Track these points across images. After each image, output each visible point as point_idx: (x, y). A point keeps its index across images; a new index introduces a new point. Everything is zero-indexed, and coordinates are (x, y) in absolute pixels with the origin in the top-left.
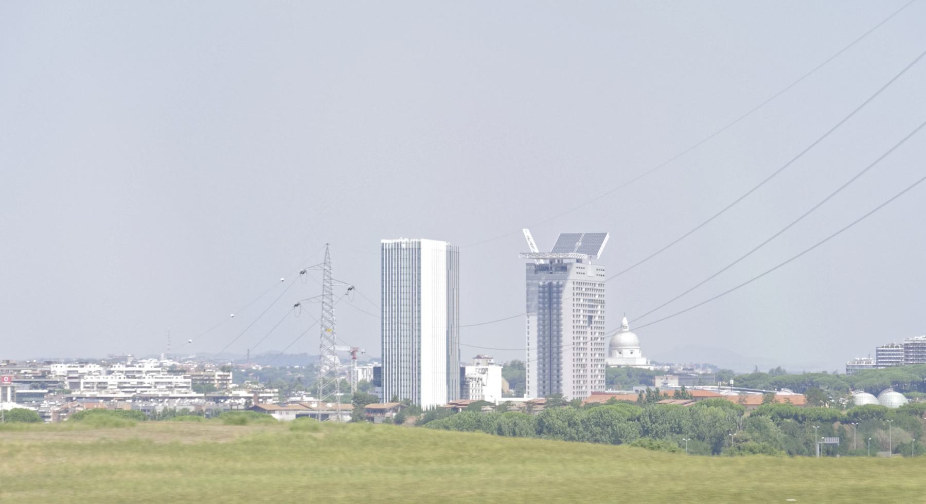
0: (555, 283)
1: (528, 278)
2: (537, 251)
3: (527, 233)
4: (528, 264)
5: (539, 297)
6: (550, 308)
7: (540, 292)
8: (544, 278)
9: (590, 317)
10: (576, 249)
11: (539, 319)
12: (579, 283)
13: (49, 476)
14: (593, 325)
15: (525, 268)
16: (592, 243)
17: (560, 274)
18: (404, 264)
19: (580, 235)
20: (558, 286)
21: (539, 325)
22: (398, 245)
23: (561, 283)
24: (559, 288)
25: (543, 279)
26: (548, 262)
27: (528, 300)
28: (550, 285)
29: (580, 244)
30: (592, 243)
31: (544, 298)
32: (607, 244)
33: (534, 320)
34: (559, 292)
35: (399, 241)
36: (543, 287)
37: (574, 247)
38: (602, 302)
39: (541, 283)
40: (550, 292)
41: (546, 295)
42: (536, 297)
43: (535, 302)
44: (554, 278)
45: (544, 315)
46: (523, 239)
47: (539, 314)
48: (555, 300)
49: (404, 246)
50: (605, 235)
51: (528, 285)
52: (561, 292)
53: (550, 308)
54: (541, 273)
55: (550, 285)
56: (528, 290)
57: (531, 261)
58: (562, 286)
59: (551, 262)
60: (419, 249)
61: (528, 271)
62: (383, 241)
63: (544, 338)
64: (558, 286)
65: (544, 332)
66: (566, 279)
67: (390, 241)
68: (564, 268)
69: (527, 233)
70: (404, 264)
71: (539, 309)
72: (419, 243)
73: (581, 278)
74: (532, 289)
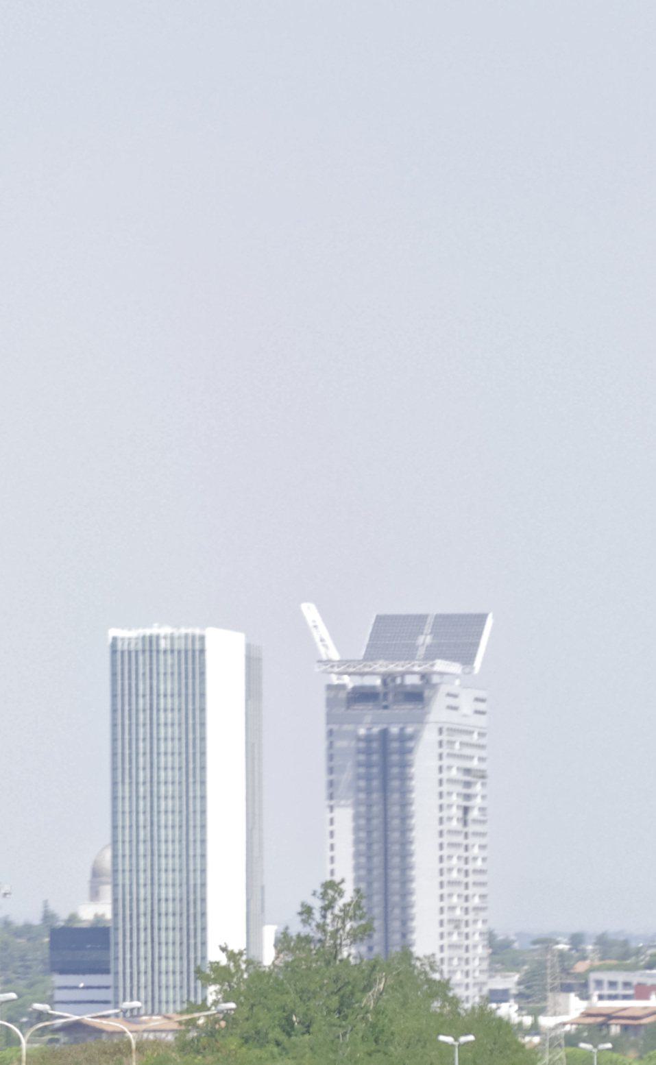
0: (394, 730)
1: (330, 718)
2: (335, 655)
3: (310, 612)
4: (330, 687)
5: (359, 764)
6: (385, 788)
7: (359, 751)
8: (368, 719)
9: (466, 810)
10: (421, 652)
11: (357, 817)
12: (452, 731)
13: (555, 1004)
14: (472, 828)
15: (321, 697)
16: (459, 635)
17: (406, 708)
18: (167, 685)
19: (422, 619)
20: (403, 738)
21: (357, 829)
22: (151, 643)
23: (409, 730)
24: (406, 743)
25: (367, 723)
26: (377, 682)
27: (331, 770)
28: (384, 733)
29: (429, 640)
30: (459, 635)
31: (368, 765)
32: (491, 637)
33: (345, 817)
34: (405, 752)
35: (148, 632)
36: (368, 739)
37: (414, 648)
38: (483, 776)
39: (362, 731)
40: (385, 753)
41: (375, 758)
42: (349, 764)
43: (346, 777)
44: (394, 720)
45: (369, 806)
46: (304, 631)
47: (357, 804)
48: (395, 770)
49: (163, 644)
50: (480, 619)
51: (330, 733)
52: (410, 751)
53: (385, 788)
54: (359, 708)
55: (384, 733)
56: (331, 745)
57: (335, 680)
58: (412, 738)
59: (384, 683)
60: (202, 651)
61: (330, 703)
62: (113, 632)
63: (369, 858)
64: (403, 738)
65: (369, 845)
66: (421, 721)
67: (133, 633)
68: (416, 697)
69: (310, 612)
70: (167, 685)
71: (359, 790)
72: (202, 638)
73: (452, 718)
74: (341, 744)
